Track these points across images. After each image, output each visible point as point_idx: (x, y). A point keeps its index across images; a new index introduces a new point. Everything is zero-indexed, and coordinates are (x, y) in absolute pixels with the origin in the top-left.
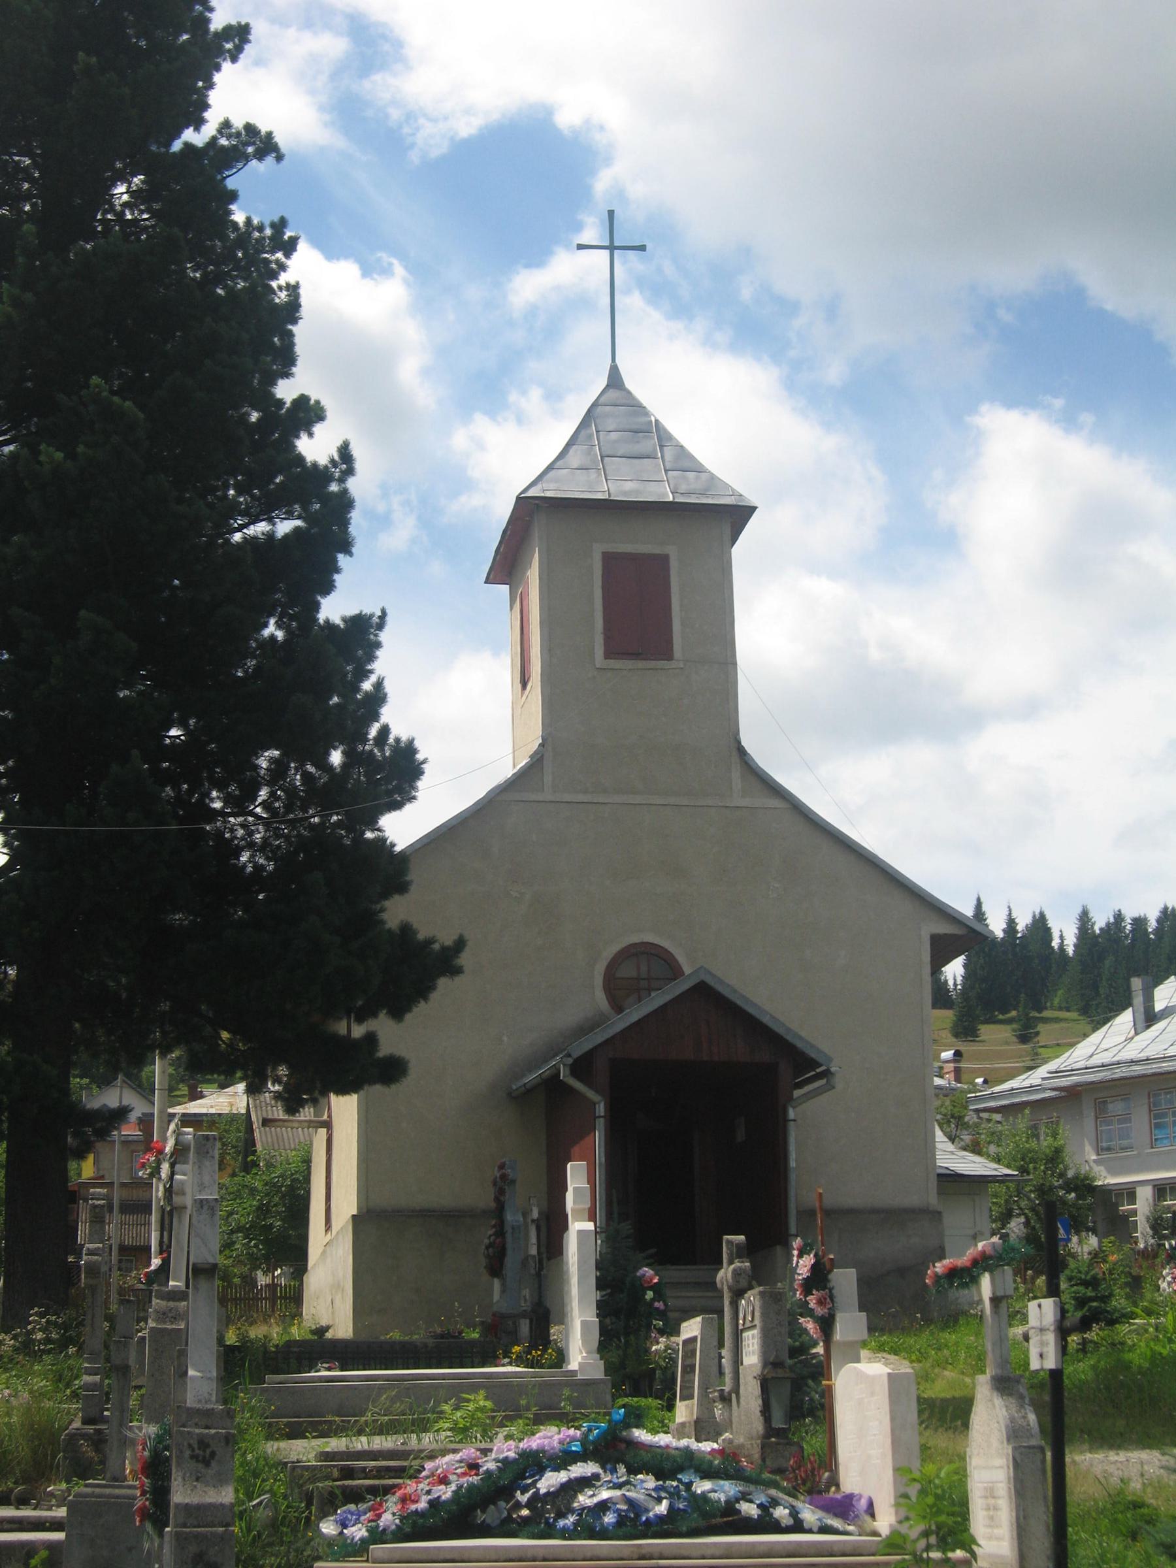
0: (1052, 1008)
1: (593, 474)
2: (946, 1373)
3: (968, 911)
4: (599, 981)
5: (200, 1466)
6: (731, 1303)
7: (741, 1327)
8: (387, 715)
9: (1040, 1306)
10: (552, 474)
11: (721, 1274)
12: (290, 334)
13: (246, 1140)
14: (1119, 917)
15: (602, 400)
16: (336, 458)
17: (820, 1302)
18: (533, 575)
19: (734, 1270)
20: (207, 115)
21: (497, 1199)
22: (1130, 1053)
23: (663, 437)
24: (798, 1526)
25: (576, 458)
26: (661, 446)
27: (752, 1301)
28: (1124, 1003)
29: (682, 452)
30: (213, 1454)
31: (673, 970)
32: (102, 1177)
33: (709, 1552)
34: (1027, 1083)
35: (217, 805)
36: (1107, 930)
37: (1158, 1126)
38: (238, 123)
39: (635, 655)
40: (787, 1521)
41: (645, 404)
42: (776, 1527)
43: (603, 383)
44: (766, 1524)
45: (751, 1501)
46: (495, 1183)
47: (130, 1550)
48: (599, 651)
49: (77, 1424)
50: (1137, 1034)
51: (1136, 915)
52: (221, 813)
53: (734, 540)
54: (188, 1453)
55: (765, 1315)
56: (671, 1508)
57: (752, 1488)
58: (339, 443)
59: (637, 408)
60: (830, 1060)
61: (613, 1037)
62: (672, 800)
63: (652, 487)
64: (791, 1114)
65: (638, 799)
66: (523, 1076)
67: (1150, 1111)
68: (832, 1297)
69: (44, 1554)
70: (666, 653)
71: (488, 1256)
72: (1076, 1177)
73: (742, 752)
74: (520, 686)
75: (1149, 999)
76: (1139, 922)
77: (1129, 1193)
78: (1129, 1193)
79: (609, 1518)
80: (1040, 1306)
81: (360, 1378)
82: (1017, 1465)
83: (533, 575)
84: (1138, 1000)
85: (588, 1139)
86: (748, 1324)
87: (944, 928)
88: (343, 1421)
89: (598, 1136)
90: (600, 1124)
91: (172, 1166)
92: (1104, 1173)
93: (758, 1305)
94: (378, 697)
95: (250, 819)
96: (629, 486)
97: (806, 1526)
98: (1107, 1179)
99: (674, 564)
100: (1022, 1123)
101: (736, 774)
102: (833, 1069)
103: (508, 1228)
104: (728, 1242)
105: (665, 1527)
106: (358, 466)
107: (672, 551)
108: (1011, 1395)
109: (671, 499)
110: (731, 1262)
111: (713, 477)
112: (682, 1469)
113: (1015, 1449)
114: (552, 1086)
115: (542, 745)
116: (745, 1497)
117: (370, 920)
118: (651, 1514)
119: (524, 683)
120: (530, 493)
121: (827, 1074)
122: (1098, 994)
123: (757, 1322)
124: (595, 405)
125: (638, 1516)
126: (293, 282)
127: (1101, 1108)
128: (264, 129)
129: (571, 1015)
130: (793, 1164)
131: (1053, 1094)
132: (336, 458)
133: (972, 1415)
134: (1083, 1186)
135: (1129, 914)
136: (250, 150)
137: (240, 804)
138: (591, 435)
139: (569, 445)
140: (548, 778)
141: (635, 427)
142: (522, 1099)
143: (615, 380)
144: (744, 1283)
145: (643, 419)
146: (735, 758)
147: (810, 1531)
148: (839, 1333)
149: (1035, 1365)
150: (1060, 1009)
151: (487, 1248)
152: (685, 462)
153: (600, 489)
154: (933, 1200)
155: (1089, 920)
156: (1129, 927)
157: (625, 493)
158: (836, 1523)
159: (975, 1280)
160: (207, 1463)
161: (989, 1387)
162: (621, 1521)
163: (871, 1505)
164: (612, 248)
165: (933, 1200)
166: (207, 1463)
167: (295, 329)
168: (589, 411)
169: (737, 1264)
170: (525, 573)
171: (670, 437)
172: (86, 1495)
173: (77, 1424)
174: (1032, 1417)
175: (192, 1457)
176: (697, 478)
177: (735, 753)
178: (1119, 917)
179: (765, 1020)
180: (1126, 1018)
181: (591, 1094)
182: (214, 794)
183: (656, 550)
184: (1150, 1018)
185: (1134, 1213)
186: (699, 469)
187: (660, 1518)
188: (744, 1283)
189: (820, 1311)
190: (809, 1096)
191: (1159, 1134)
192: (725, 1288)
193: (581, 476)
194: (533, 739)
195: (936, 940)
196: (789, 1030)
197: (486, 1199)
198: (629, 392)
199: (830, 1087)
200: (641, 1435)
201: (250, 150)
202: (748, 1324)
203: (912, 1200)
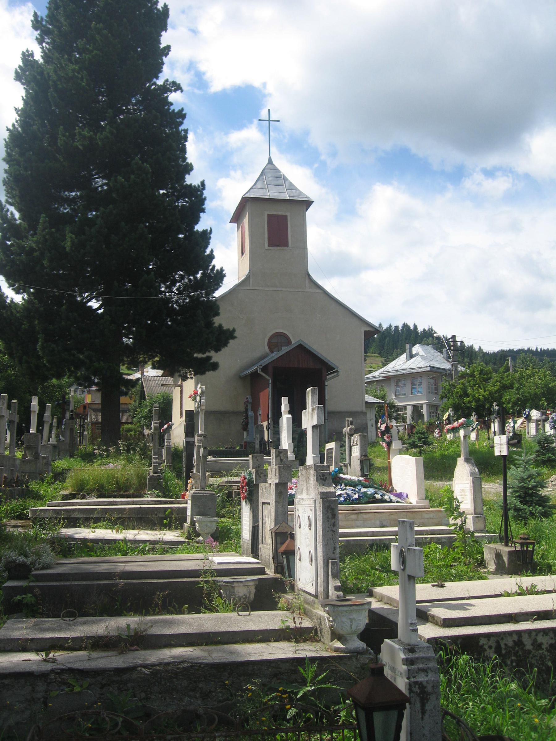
0: (370, 353)
1: (264, 190)
2: (378, 460)
3: (377, 325)
4: (266, 343)
5: (323, 481)
6: (348, 438)
7: (351, 445)
8: (214, 262)
9: (500, 437)
10: (252, 190)
11: (345, 429)
12: (185, 145)
13: (141, 391)
14: (390, 326)
15: (267, 167)
16: (200, 185)
17: (388, 438)
18: (246, 221)
19: (350, 428)
20: (160, 75)
21: (245, 408)
22: (406, 366)
23: (285, 179)
24: (391, 501)
25: (259, 185)
26: (285, 182)
27: (356, 438)
28: (403, 352)
29: (291, 184)
30: (326, 478)
31: (288, 342)
32: (94, 402)
33: (372, 508)
34: (374, 375)
35: (163, 289)
36: (387, 329)
37: (414, 388)
38: (171, 80)
39: (278, 246)
40: (388, 500)
41: (279, 169)
42: (385, 501)
43: (267, 162)
44: (383, 501)
45: (378, 494)
46: (245, 403)
47: (210, 508)
48: (266, 244)
49: (151, 474)
50: (407, 361)
51: (396, 325)
52: (164, 292)
53: (307, 211)
54: (319, 478)
55: (361, 442)
56: (359, 496)
57: (377, 490)
58: (201, 180)
59: (277, 170)
60: (338, 367)
61: (274, 360)
62: (289, 290)
63: (282, 195)
64: (326, 383)
65: (278, 289)
66: (244, 372)
67: (411, 384)
68: (391, 436)
69: (169, 510)
70: (286, 245)
71: (243, 425)
72: (390, 403)
73: (309, 275)
74: (241, 254)
75: (411, 351)
76: (396, 328)
77: (404, 408)
78: (404, 408)
79: (342, 499)
80: (500, 437)
81: (225, 460)
82: (473, 483)
83: (246, 221)
84: (408, 351)
85: (266, 391)
86: (354, 444)
87: (368, 329)
88: (226, 473)
89: (269, 389)
90: (270, 386)
91: (200, 397)
92: (398, 402)
93: (359, 438)
94: (211, 257)
95: (173, 294)
96: (275, 194)
97: (393, 501)
98: (398, 404)
99: (289, 218)
100: (374, 386)
101: (307, 281)
102: (339, 370)
103: (249, 416)
104: (348, 420)
105: (358, 501)
106: (206, 187)
107: (288, 214)
108: (470, 463)
109: (288, 198)
110: (348, 426)
111: (301, 192)
112: (357, 485)
113: (473, 478)
114: (255, 376)
115: (249, 272)
116: (376, 493)
117: (210, 324)
118: (353, 498)
119: (243, 254)
120: (246, 196)
121: (337, 371)
122: (384, 349)
123: (358, 443)
124: (264, 169)
125: (350, 498)
126: (186, 128)
127: (397, 382)
128: (178, 82)
129: (258, 354)
130: (326, 398)
131: (381, 378)
132: (200, 185)
133: (456, 469)
134: (391, 406)
135: (393, 325)
136: (173, 89)
137: (169, 288)
138: (263, 178)
139: (257, 181)
140: (251, 282)
141: (277, 176)
142: (243, 378)
143: (270, 162)
144: (353, 432)
145: (279, 174)
146: (307, 277)
147: (394, 503)
148: (393, 447)
149: (497, 453)
150: (372, 353)
151: (243, 422)
152: (292, 187)
153: (268, 195)
154: (364, 409)
155: (382, 326)
156: (393, 329)
157: (275, 196)
158: (399, 500)
159: (458, 432)
160: (325, 481)
161: (463, 461)
162: (345, 500)
163: (407, 496)
164: (269, 121)
165: (364, 409)
166: (325, 481)
167: (186, 143)
168: (263, 171)
169: (350, 427)
170: (243, 220)
171: (287, 179)
172: (197, 493)
173: (151, 474)
174: (476, 469)
175: (321, 479)
176: (296, 192)
177: (307, 276)
178: (390, 326)
179: (319, 355)
180: (404, 357)
181: (267, 377)
182: (162, 285)
183: (284, 214)
184: (411, 356)
185: (406, 414)
186: (296, 189)
187: (356, 499)
188: (353, 432)
189: (387, 440)
190: (331, 378)
191: (413, 391)
192: (346, 434)
193: (261, 191)
194: (247, 271)
195: (366, 333)
196: (326, 359)
197: (242, 408)
198: (274, 165)
199: (338, 375)
200: (341, 475)
201: (173, 89)
202: (354, 444)
203: (358, 409)
